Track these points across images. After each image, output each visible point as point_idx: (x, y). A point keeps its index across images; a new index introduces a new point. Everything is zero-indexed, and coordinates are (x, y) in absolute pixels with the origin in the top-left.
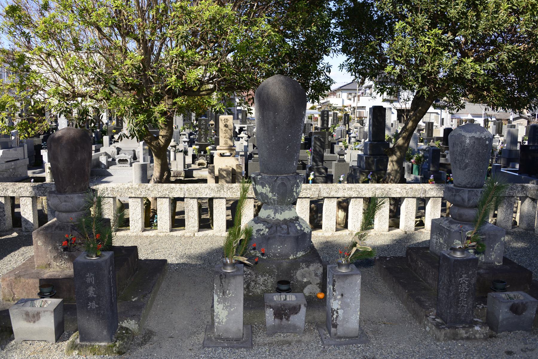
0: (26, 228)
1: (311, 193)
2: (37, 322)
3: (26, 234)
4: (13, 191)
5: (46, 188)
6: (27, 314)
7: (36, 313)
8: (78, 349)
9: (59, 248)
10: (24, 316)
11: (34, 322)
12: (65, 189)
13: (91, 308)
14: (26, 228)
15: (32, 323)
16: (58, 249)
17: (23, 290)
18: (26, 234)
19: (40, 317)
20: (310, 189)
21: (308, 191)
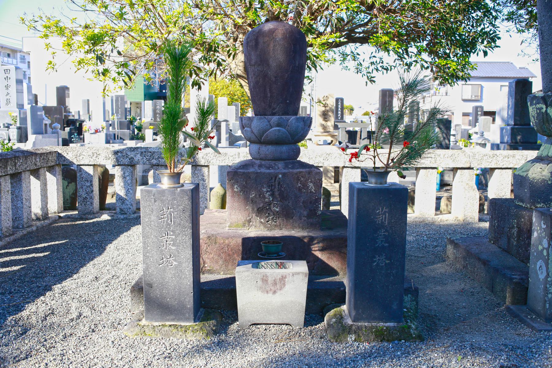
0: (121, 210)
1: (514, 162)
2: (279, 292)
3: (122, 217)
4: (106, 157)
5: (154, 152)
6: (265, 280)
7: (280, 277)
8: (355, 333)
9: (267, 195)
10: (260, 283)
11: (275, 292)
12: (274, 109)
13: (378, 265)
14: (121, 210)
15: (270, 295)
16: (264, 197)
17: (219, 255)
18: (122, 217)
19: (284, 285)
20: (514, 156)
21: (511, 159)
